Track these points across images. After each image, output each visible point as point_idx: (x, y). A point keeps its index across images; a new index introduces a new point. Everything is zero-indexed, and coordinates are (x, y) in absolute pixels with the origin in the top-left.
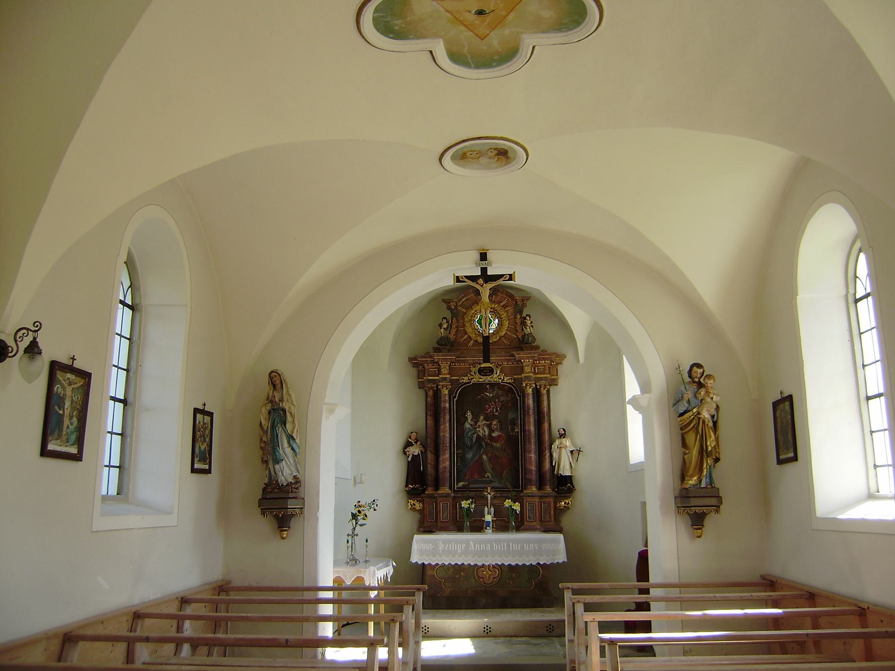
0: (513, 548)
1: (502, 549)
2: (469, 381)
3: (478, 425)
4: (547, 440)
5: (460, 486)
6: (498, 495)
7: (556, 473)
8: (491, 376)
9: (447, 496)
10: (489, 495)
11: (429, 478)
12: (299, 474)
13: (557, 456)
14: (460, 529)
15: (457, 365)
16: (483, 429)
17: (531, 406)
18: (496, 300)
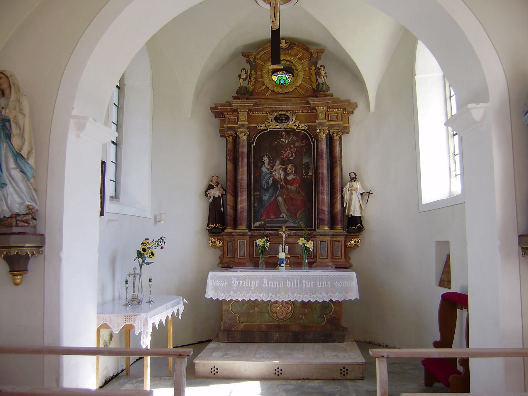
0: (306, 285)
1: (296, 286)
2: (266, 128)
3: (274, 169)
4: (338, 183)
5: (257, 226)
6: (292, 234)
7: (346, 214)
8: (287, 123)
9: (244, 234)
10: (284, 234)
11: (229, 218)
12: (36, 203)
13: (348, 198)
14: (256, 265)
15: (256, 114)
16: (279, 173)
17: (324, 150)
18: (292, 54)
